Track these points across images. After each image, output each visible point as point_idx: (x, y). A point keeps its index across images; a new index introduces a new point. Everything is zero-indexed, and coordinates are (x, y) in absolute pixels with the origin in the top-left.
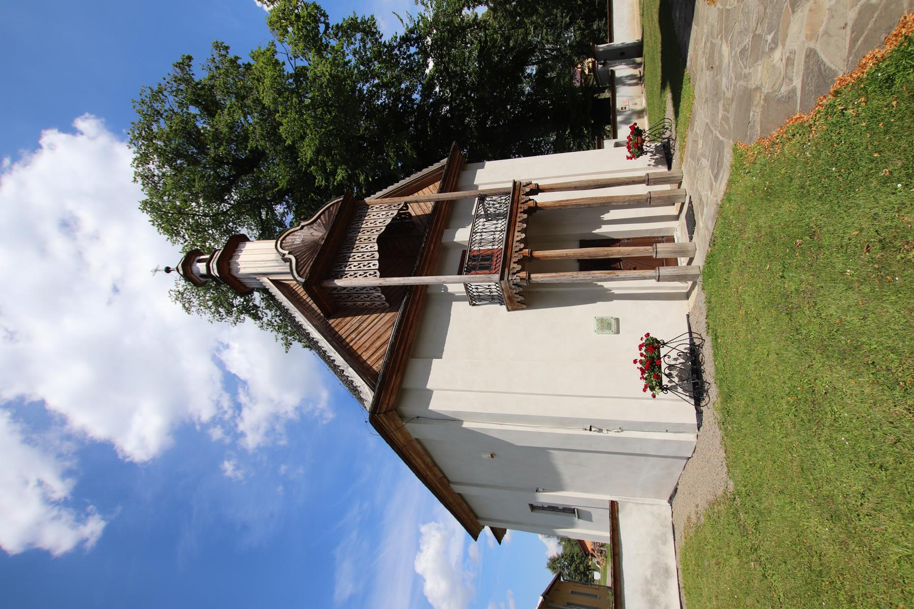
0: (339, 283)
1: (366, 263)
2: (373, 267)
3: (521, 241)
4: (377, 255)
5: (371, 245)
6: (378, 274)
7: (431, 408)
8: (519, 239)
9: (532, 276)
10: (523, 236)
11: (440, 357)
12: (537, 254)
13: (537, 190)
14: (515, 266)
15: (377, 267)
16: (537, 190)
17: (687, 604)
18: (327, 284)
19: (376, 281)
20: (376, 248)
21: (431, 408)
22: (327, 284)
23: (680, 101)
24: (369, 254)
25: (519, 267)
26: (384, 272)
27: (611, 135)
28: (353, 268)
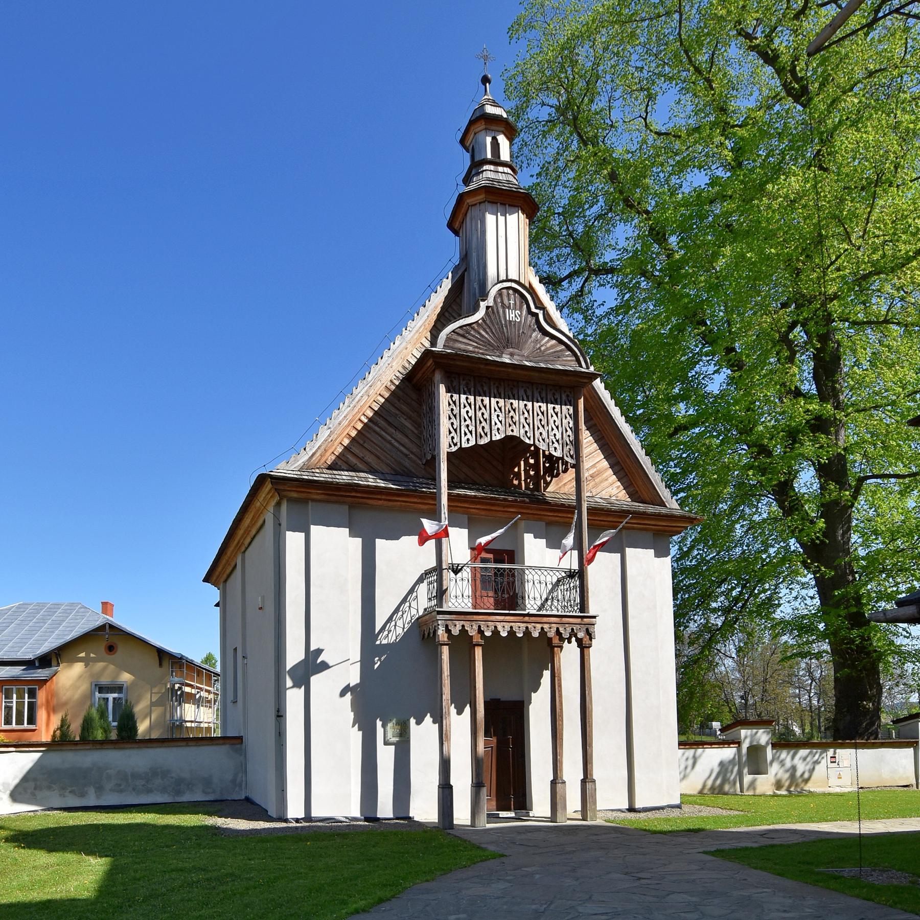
0: (444, 396)
1: (472, 428)
2: (464, 439)
3: (496, 632)
4: (484, 441)
5: (502, 429)
6: (454, 449)
7: (377, 540)
8: (500, 628)
9: (480, 648)
10: (504, 634)
11: (535, 537)
12: (478, 652)
13: (584, 647)
14: (459, 627)
15: (465, 445)
16: (584, 647)
17: (100, 789)
18: (438, 376)
19: (445, 446)
20: (497, 437)
21: (377, 540)
22: (438, 376)
23: (51, 849)
24: (487, 429)
25: (456, 631)
26: (458, 458)
27: (684, 738)
28: (463, 411)
